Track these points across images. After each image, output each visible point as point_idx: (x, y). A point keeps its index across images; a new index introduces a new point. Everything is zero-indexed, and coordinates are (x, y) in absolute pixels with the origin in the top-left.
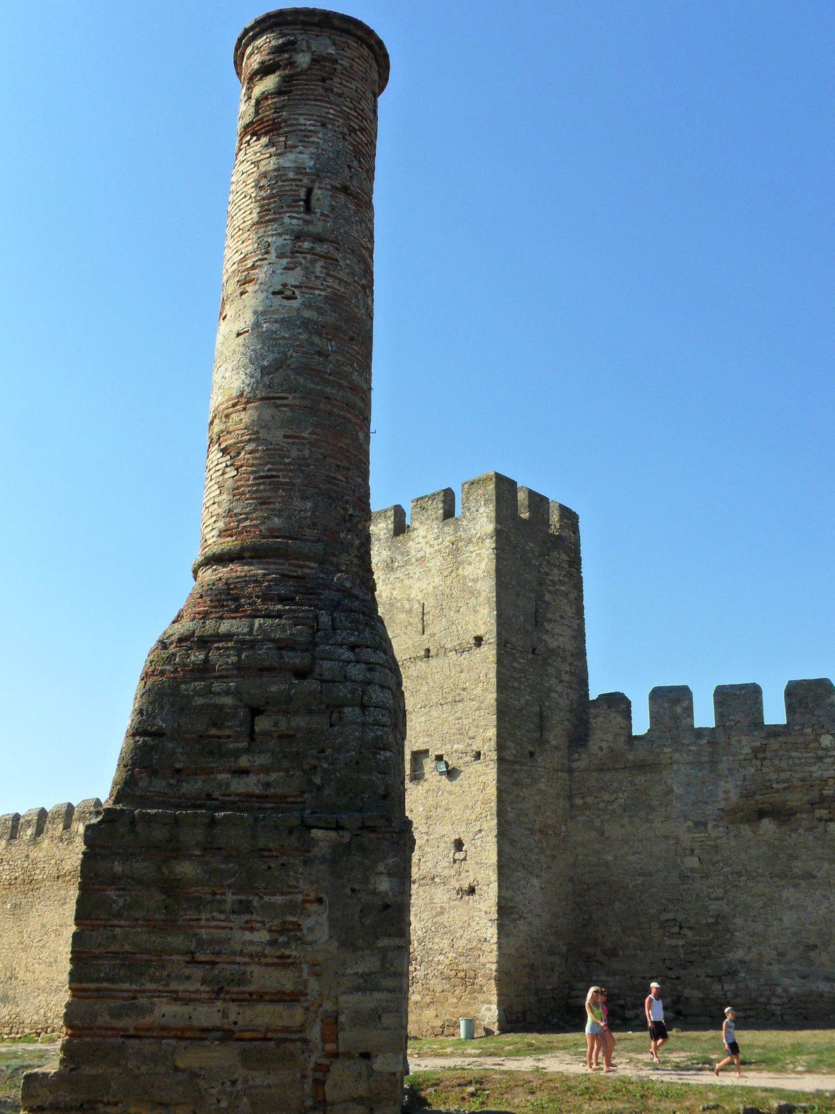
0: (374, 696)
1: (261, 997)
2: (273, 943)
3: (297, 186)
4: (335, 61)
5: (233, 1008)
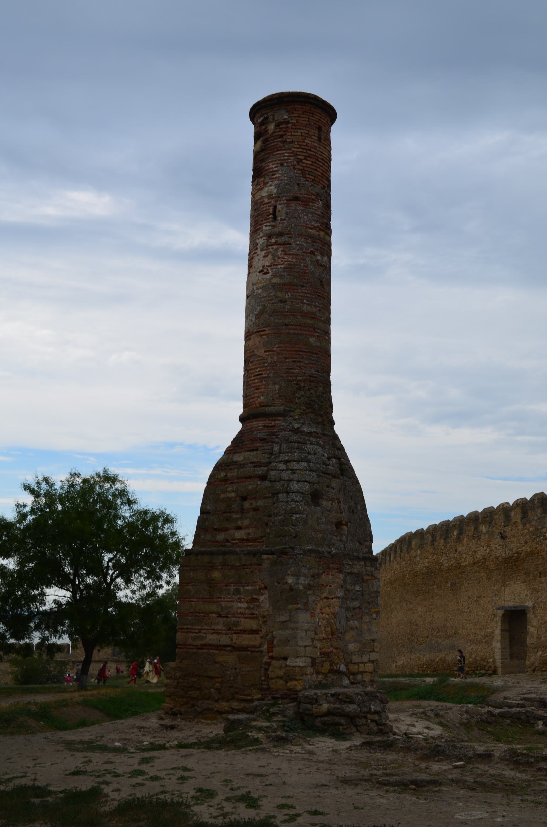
0: (292, 487)
1: (244, 632)
2: (248, 608)
3: (269, 206)
4: (288, 122)
5: (235, 636)
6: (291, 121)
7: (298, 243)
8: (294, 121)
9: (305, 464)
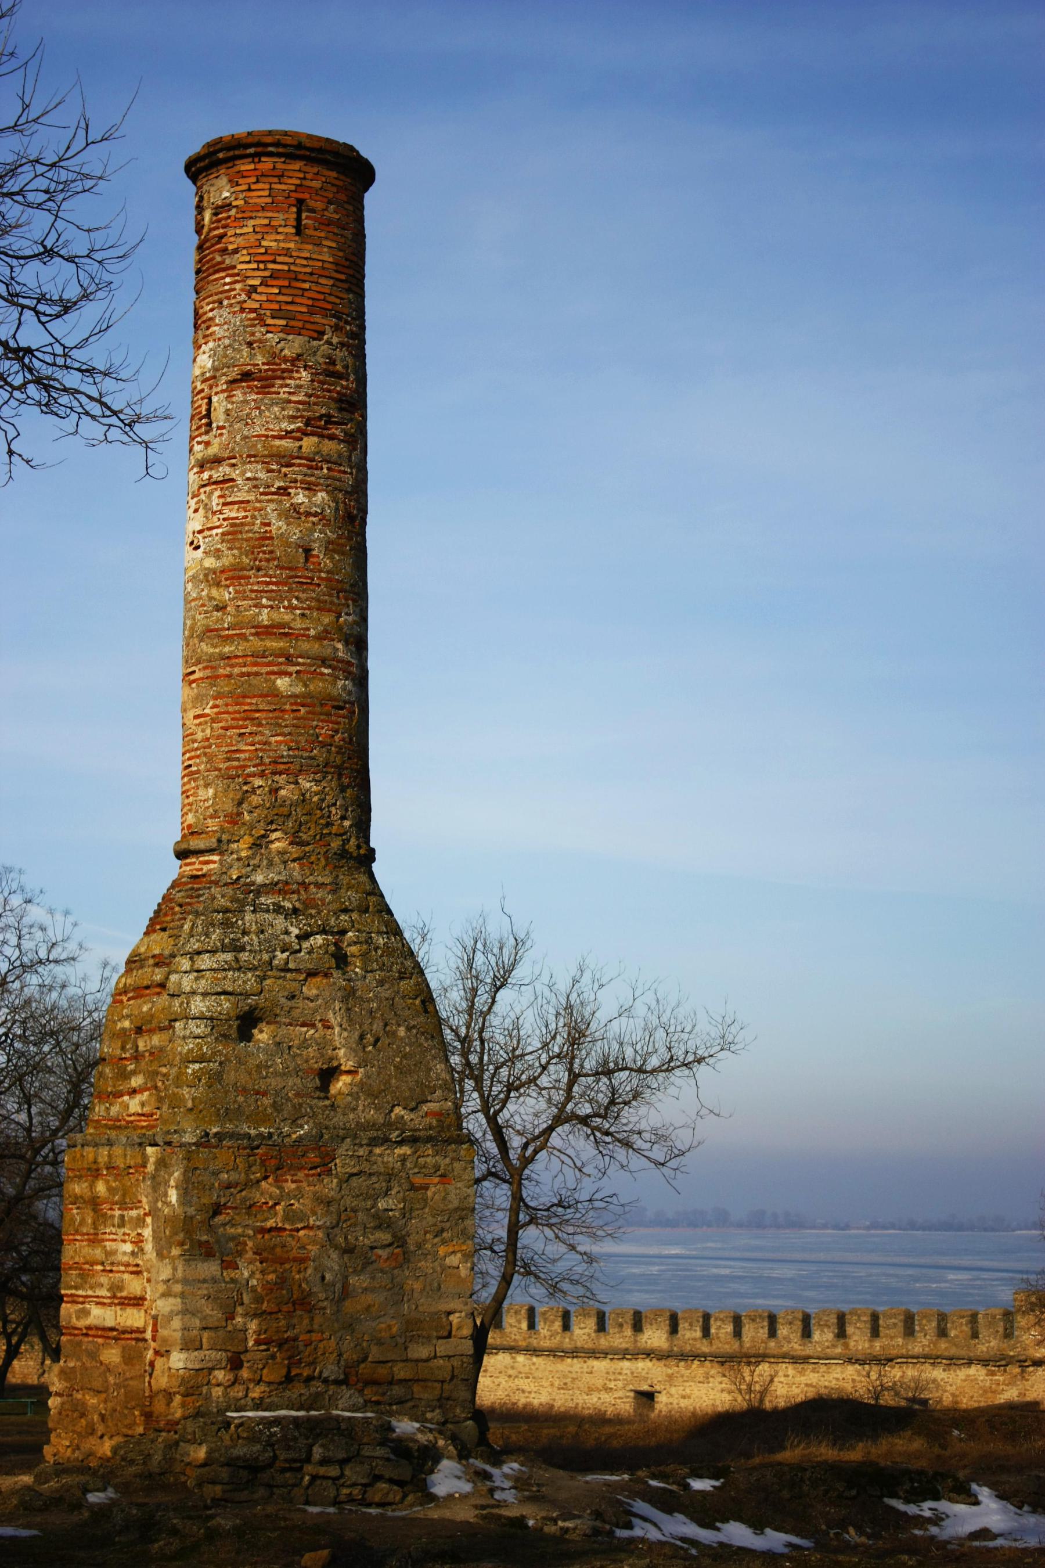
6: (234, 203)
7: (249, 475)
8: (240, 203)
9: (229, 956)
